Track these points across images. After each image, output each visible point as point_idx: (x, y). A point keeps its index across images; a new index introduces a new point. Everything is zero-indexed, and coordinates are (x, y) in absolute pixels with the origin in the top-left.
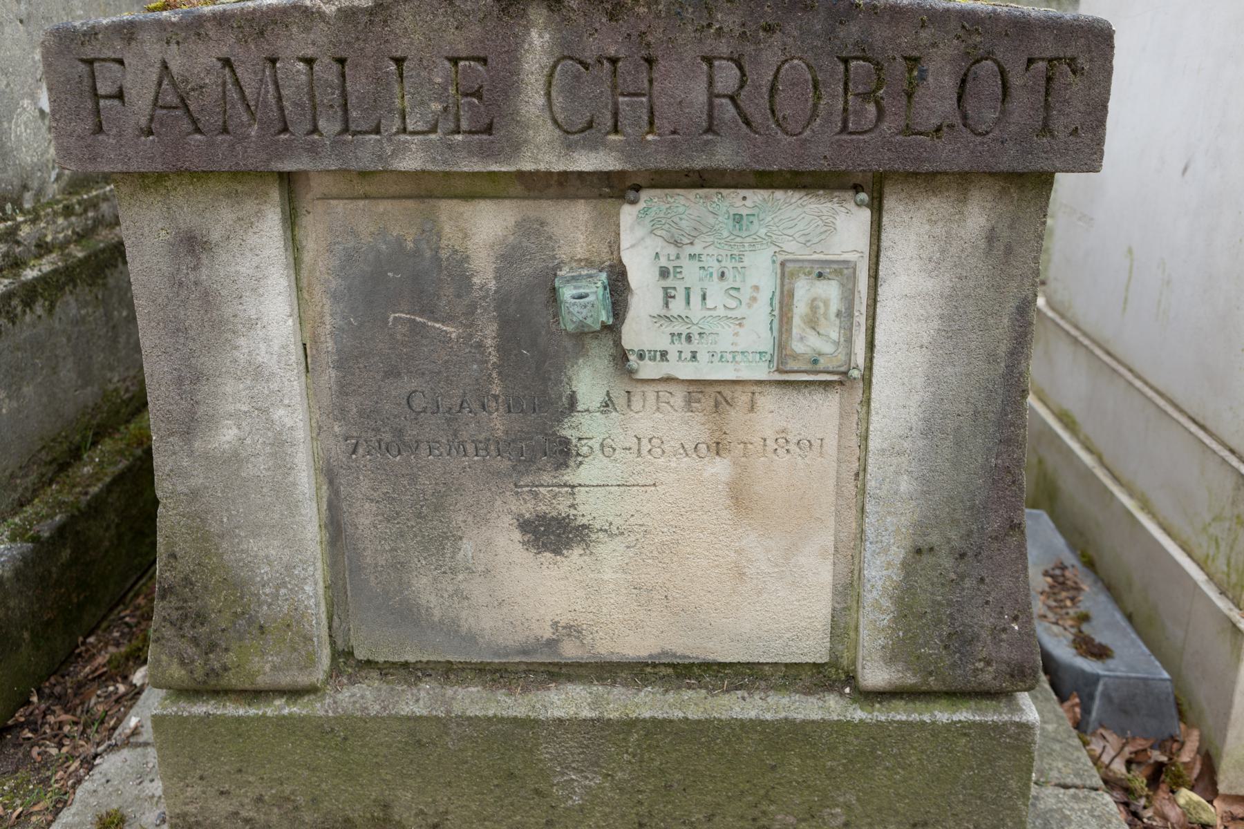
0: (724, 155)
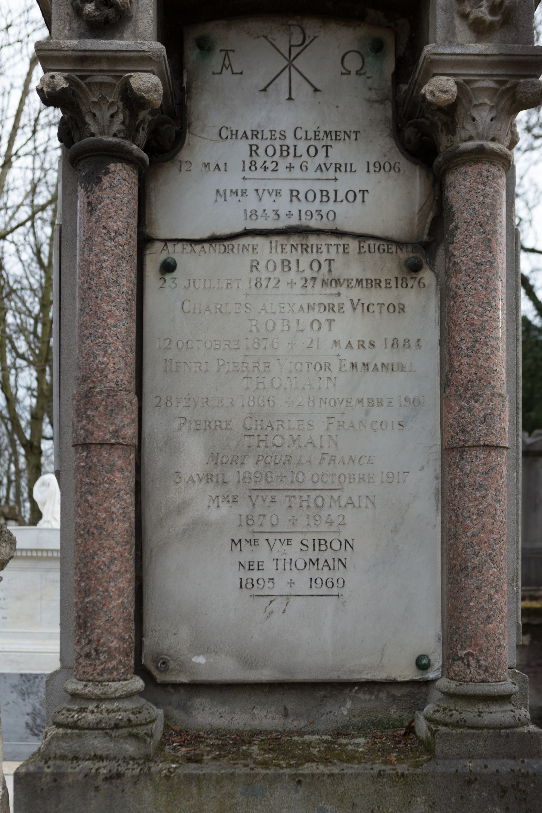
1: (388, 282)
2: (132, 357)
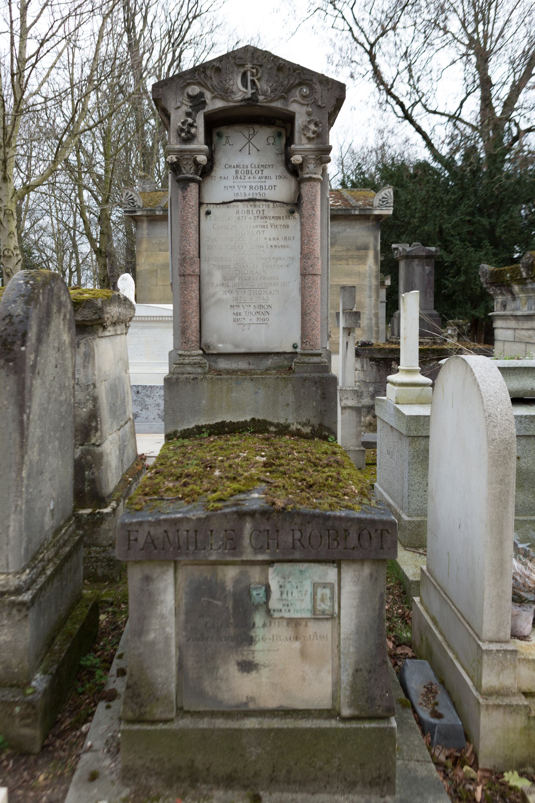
0: (297, 555)
1: (283, 217)
2: (198, 246)
